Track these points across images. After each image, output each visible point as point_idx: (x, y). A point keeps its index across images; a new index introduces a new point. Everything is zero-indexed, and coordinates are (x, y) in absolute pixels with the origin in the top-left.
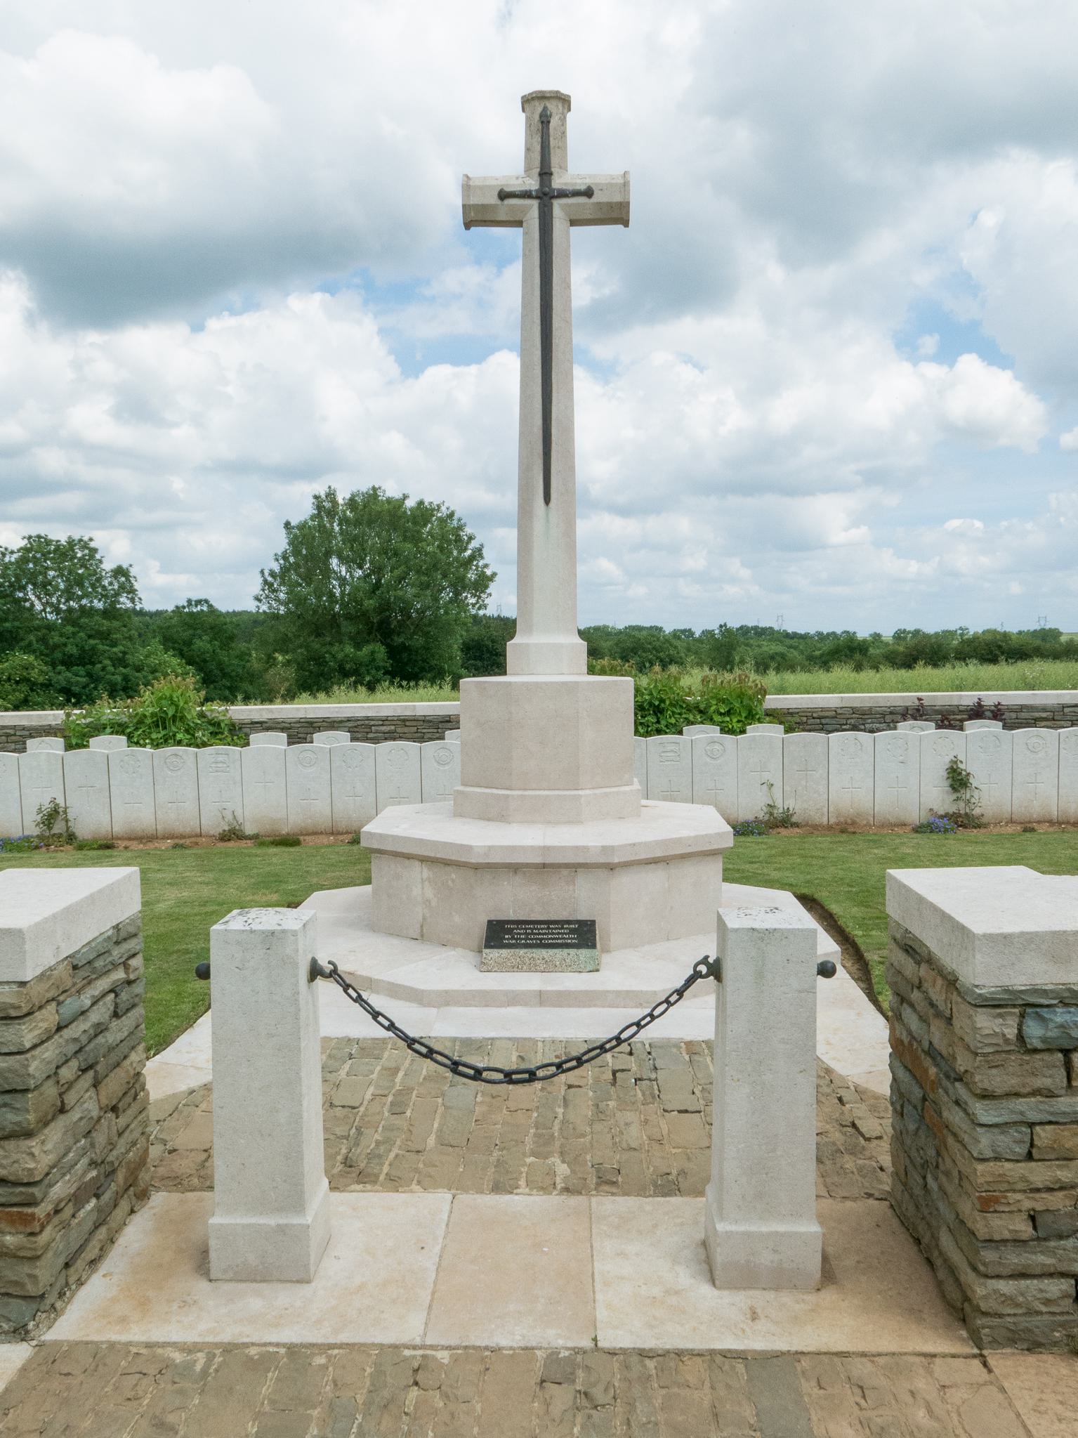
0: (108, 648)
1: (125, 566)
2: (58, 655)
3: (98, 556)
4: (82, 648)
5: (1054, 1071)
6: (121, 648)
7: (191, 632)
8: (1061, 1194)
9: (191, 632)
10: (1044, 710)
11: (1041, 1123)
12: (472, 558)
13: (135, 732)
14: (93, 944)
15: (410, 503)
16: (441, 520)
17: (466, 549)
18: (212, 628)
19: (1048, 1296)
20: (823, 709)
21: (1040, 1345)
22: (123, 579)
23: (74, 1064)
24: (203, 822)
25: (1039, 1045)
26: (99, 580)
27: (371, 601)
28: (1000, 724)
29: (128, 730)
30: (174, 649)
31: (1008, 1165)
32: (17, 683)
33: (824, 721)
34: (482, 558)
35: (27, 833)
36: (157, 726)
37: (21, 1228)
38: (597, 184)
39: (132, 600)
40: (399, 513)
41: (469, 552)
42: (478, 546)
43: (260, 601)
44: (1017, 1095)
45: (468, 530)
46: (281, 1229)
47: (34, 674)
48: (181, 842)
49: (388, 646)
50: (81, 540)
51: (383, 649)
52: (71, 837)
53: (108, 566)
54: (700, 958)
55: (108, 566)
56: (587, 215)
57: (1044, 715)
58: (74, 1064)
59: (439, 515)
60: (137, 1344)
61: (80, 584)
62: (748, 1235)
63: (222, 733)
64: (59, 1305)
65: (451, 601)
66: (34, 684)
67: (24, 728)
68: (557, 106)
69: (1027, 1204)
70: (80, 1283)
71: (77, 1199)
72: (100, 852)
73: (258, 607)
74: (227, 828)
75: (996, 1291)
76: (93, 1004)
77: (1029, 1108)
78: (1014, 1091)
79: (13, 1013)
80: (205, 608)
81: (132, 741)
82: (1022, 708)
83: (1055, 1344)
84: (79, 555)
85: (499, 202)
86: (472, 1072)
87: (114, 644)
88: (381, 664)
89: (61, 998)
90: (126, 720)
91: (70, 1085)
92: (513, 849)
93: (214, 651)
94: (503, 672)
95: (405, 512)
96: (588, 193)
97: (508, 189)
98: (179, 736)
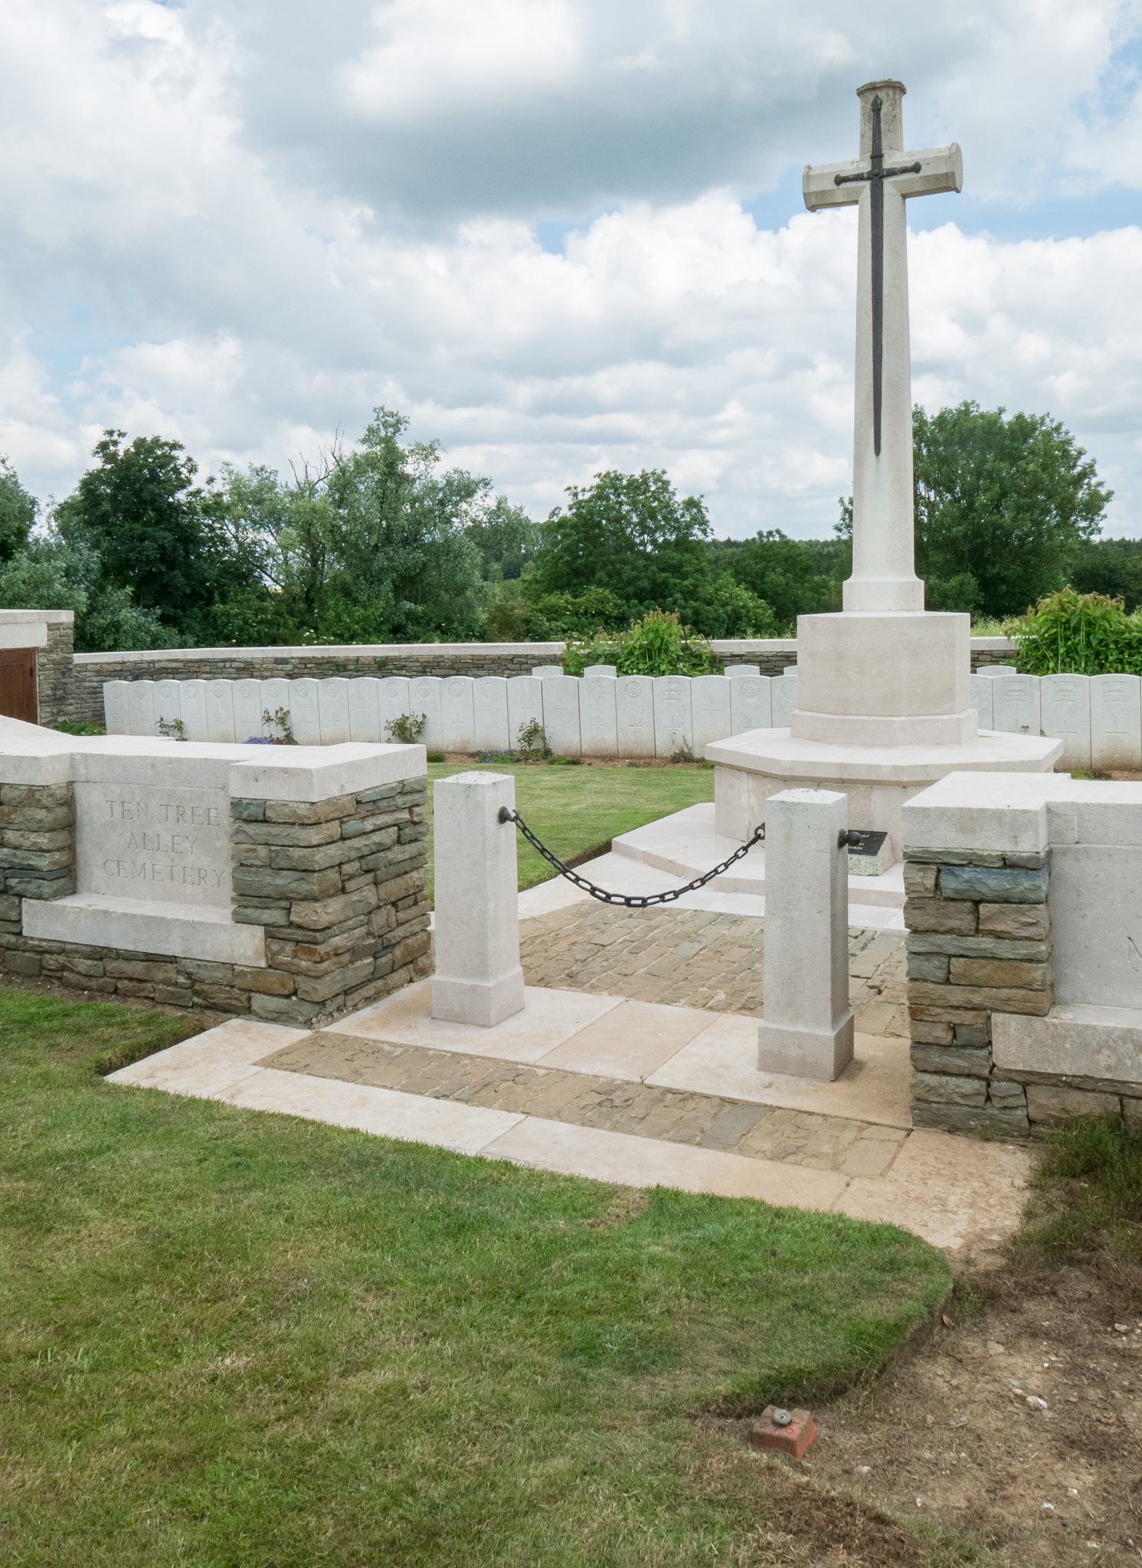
0: (678, 581)
1: (696, 498)
2: (631, 589)
3: (671, 489)
4: (654, 580)
5: (963, 916)
7: (764, 564)
8: (973, 1013)
11: (955, 956)
12: (1083, 475)
13: (622, 663)
14: (377, 790)
15: (1007, 418)
16: (1047, 435)
17: (1074, 466)
18: (786, 560)
19: (964, 1091)
21: (958, 1129)
22: (695, 510)
23: (356, 865)
24: (658, 745)
25: (953, 895)
26: (672, 512)
27: (960, 528)
29: (619, 661)
31: (932, 986)
32: (593, 616)
34: (1095, 475)
35: (513, 747)
36: (644, 658)
37: (309, 957)
38: (924, 160)
39: (704, 532)
40: (995, 429)
41: (1078, 469)
42: (1089, 461)
43: (840, 530)
44: (935, 931)
45: (1078, 444)
46: (474, 989)
47: (609, 608)
48: (634, 761)
49: (979, 576)
50: (653, 473)
52: (547, 753)
53: (680, 498)
54: (760, 824)
55: (680, 498)
56: (917, 188)
58: (356, 865)
59: (1044, 428)
60: (370, 1040)
61: (653, 517)
62: (778, 1031)
63: (702, 665)
64: (336, 1015)
65: (1058, 526)
66: (609, 617)
67: (534, 657)
68: (888, 94)
69: (946, 1018)
70: (356, 1008)
71: (356, 952)
72: (568, 767)
73: (838, 537)
74: (677, 751)
75: (922, 1081)
76: (374, 831)
77: (949, 943)
78: (933, 928)
79: (306, 822)
80: (777, 539)
81: (622, 671)
83: (971, 1130)
84: (653, 488)
85: (835, 187)
86: (604, 896)
87: (685, 577)
88: (971, 597)
89: (345, 819)
90: (619, 651)
91: (351, 877)
92: (814, 765)
93: (787, 584)
94: (838, 608)
95: (1001, 428)
96: (916, 168)
97: (842, 175)
98: (663, 667)
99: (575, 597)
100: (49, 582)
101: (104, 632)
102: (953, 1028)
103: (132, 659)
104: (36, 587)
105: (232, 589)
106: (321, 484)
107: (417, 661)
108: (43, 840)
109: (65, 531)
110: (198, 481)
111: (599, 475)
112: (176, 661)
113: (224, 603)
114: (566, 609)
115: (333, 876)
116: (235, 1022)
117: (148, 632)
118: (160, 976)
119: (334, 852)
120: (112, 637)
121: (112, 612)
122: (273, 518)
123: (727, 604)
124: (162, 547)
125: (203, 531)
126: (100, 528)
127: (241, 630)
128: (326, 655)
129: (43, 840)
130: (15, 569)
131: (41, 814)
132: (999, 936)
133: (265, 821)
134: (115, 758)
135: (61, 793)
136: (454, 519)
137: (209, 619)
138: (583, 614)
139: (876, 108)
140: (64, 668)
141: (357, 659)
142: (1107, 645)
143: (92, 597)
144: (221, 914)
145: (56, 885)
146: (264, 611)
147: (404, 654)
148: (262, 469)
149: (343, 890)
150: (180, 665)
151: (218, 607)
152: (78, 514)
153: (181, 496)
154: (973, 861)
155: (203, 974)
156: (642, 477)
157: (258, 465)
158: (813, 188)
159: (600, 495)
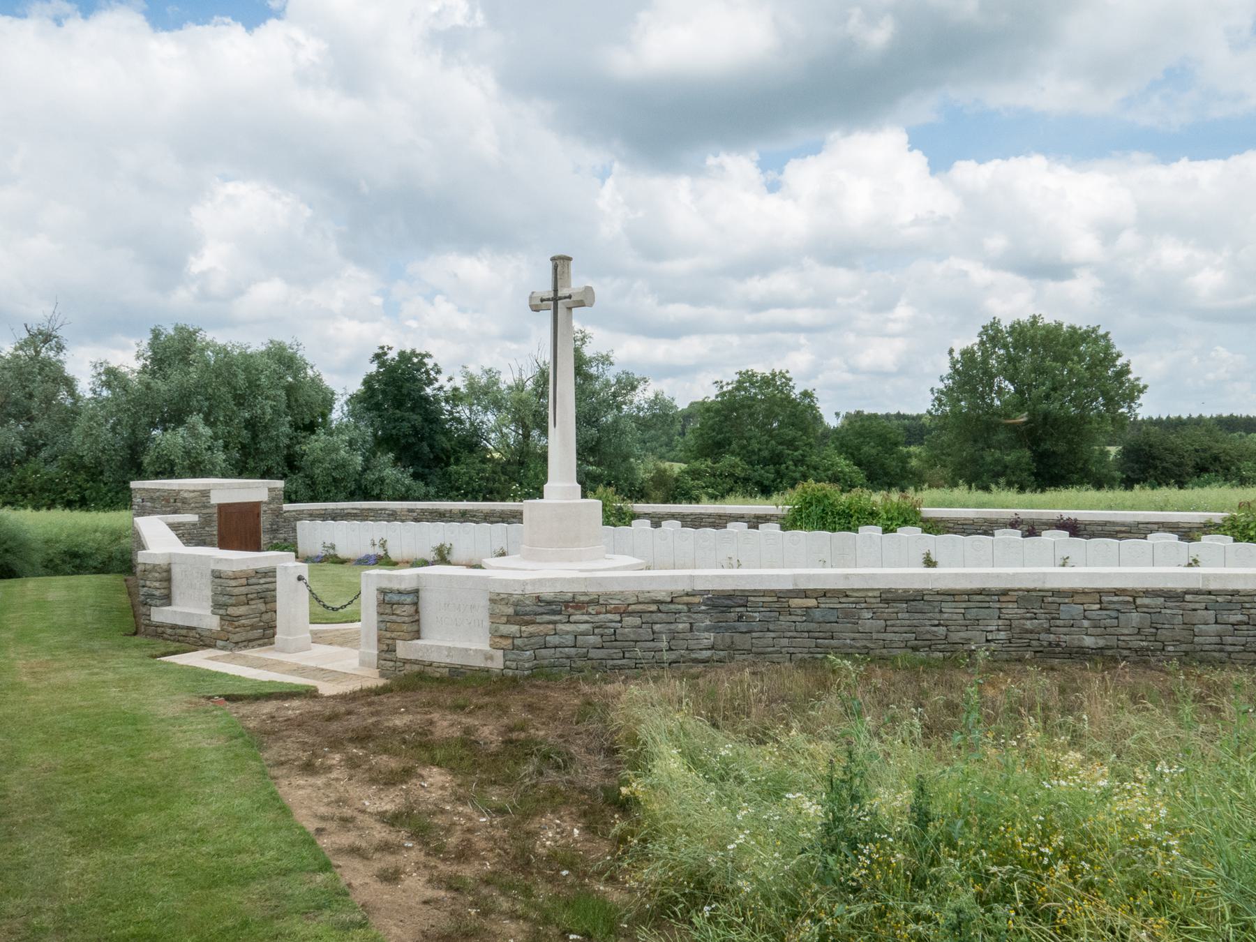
6: (801, 452)
7: (862, 439)
9: (862, 439)
10: (1123, 525)
18: (879, 436)
20: (965, 519)
23: (255, 595)
28: (44, 509)
30: (846, 453)
33: (965, 527)
46: (286, 640)
47: (738, 472)
49: (1034, 452)
51: (1028, 453)
57: (1123, 529)
66: (738, 478)
70: (253, 647)
71: (253, 627)
82: (1105, 523)
87: (796, 449)
91: (252, 600)
96: (570, 297)
99: (714, 463)
100: (337, 450)
101: (373, 484)
102: (388, 645)
103: (331, 507)
104: (329, 454)
105: (464, 454)
106: (529, 383)
107: (482, 512)
108: (157, 584)
109: (352, 413)
110: (442, 380)
111: (740, 373)
112: (356, 509)
113: (457, 465)
114: (706, 472)
115: (243, 598)
116: (211, 650)
117: (403, 484)
118: (191, 634)
119: (244, 590)
120: (378, 488)
121: (380, 471)
122: (497, 404)
123: (829, 470)
124: (413, 426)
125: (444, 415)
126: (375, 412)
127: (468, 483)
128: (435, 508)
129: (157, 584)
130: (316, 441)
131: (157, 575)
132: (397, 615)
133: (221, 578)
134: (183, 555)
135: (165, 567)
136: (623, 406)
137: (446, 476)
138: (719, 476)
139: (555, 268)
140: (278, 513)
141: (451, 511)
142: (827, 513)
143: (367, 460)
144: (208, 612)
145: (162, 601)
146: (484, 471)
147: (475, 508)
148: (490, 370)
149: (248, 604)
150: (358, 511)
151: (453, 468)
152: (360, 402)
153: (429, 391)
154: (391, 592)
155: (203, 633)
156: (771, 374)
157: (487, 368)
158: (533, 303)
159: (740, 386)
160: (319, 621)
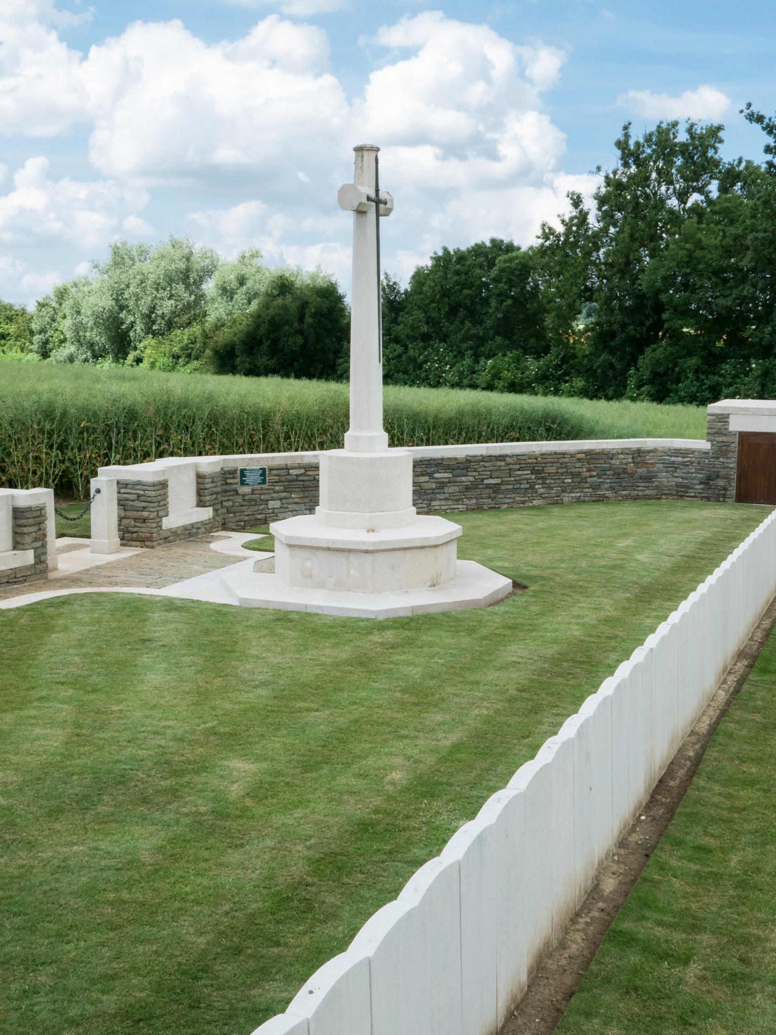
160: (264, 548)
